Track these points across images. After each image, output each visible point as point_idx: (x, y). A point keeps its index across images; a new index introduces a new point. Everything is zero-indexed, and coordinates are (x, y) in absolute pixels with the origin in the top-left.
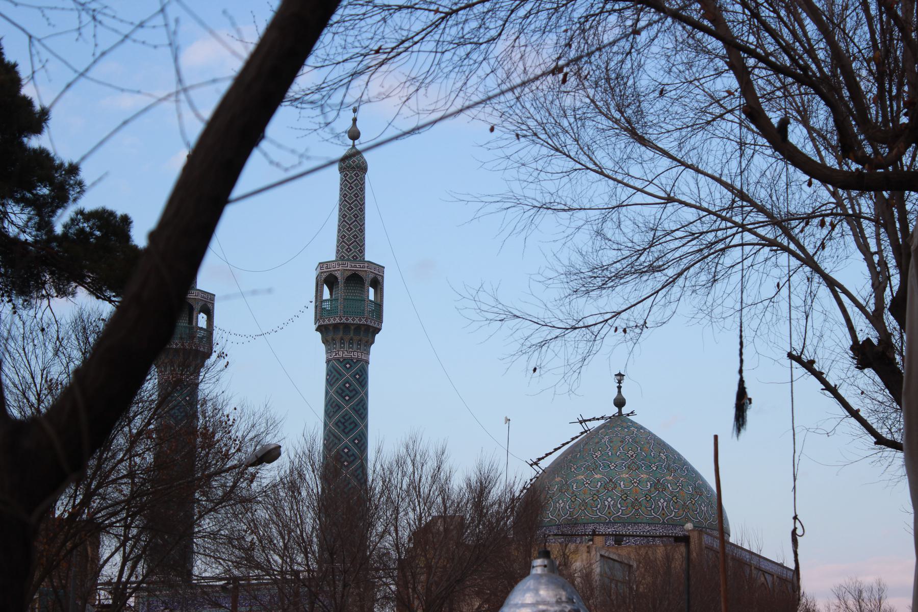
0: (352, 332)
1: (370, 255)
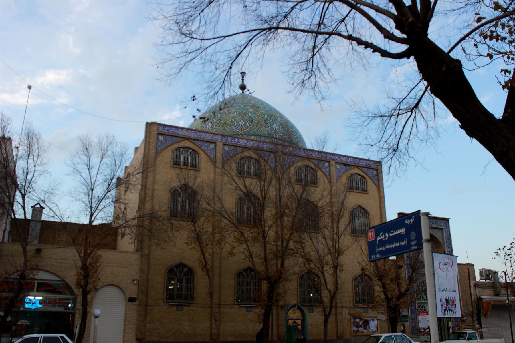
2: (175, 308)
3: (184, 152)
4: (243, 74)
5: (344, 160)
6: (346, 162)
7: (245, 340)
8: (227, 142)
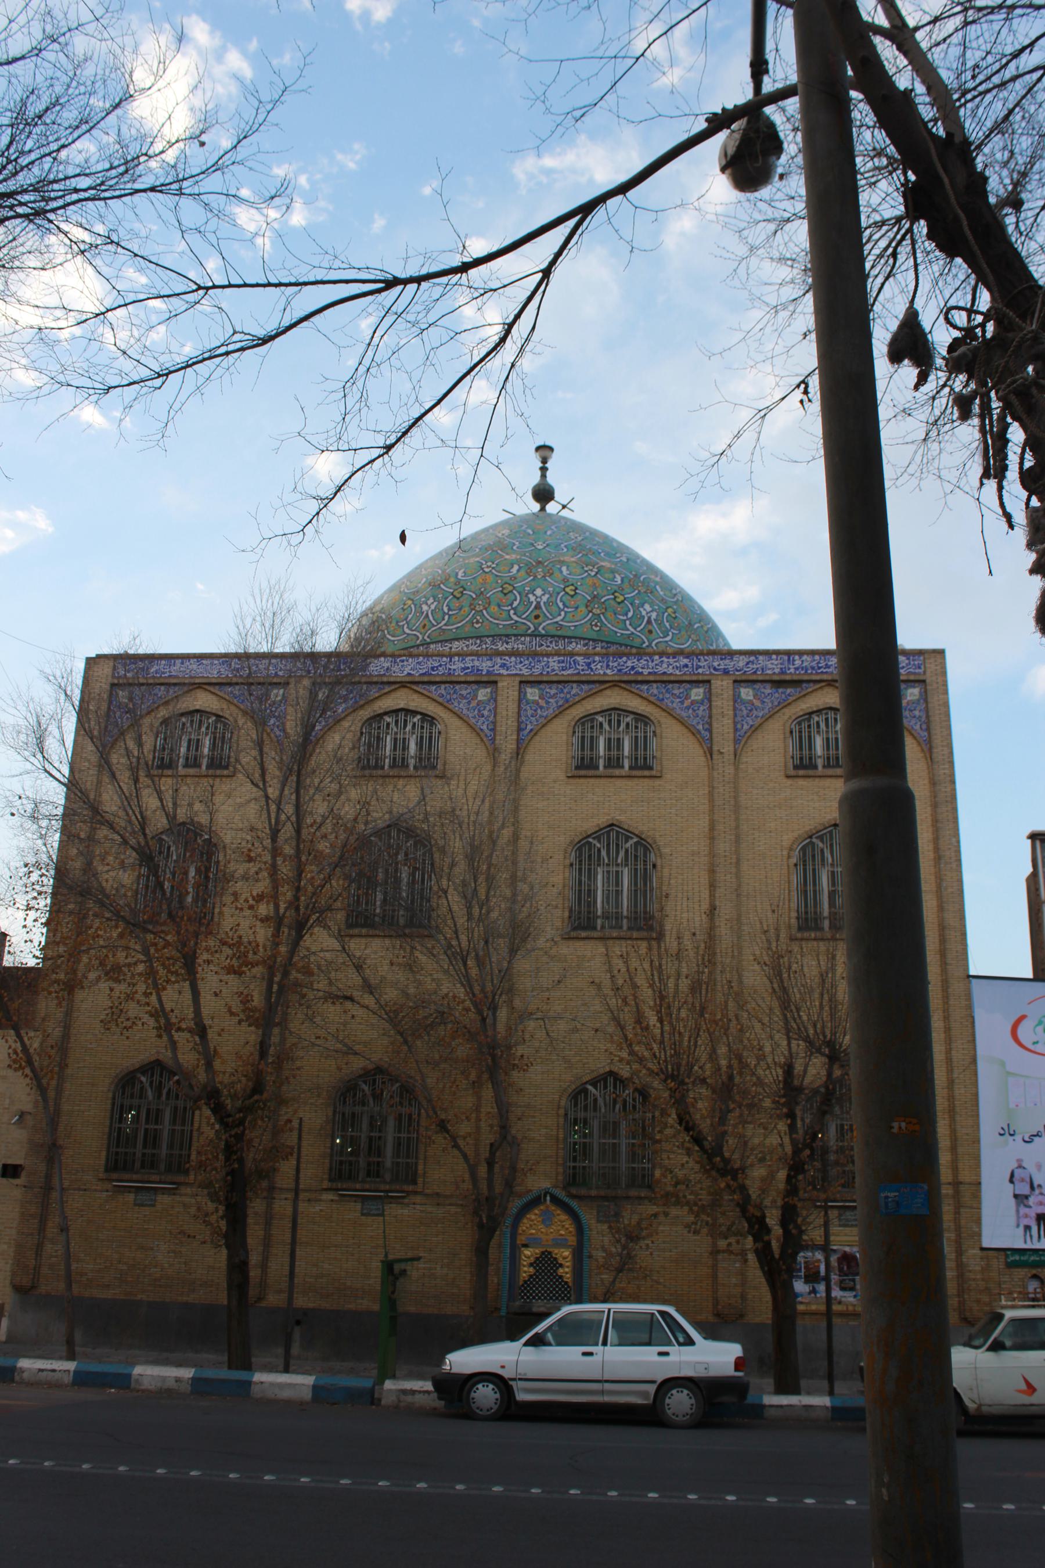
2: (131, 1197)
3: (606, 726)
4: (544, 451)
5: (773, 668)
6: (783, 672)
7: (352, 1307)
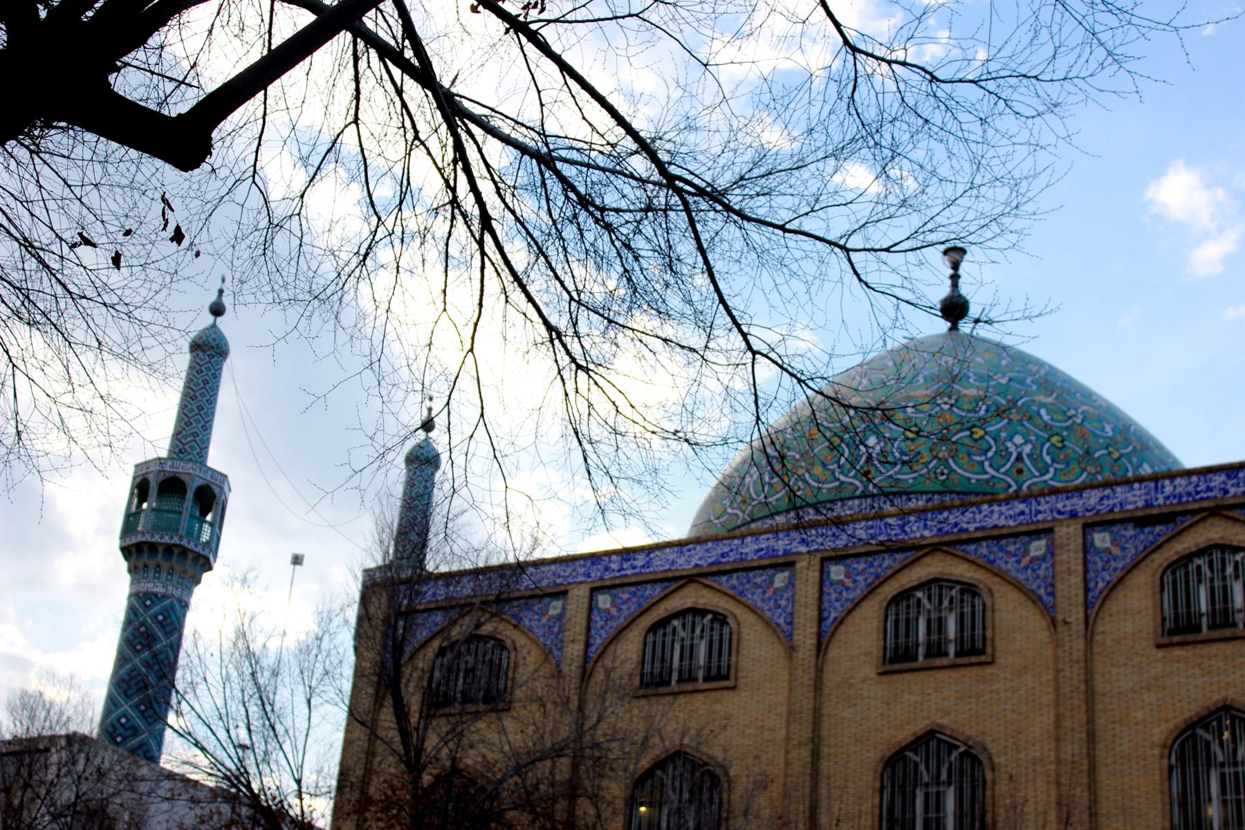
0: (160, 556)
1: (216, 459)
8: (607, 576)
